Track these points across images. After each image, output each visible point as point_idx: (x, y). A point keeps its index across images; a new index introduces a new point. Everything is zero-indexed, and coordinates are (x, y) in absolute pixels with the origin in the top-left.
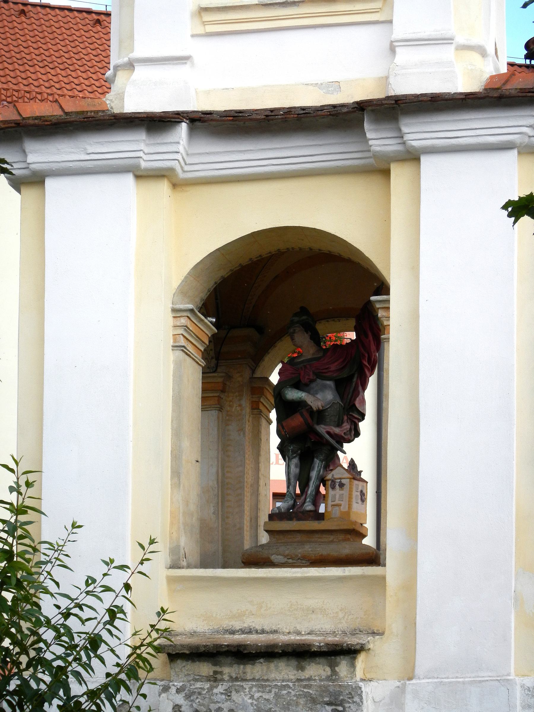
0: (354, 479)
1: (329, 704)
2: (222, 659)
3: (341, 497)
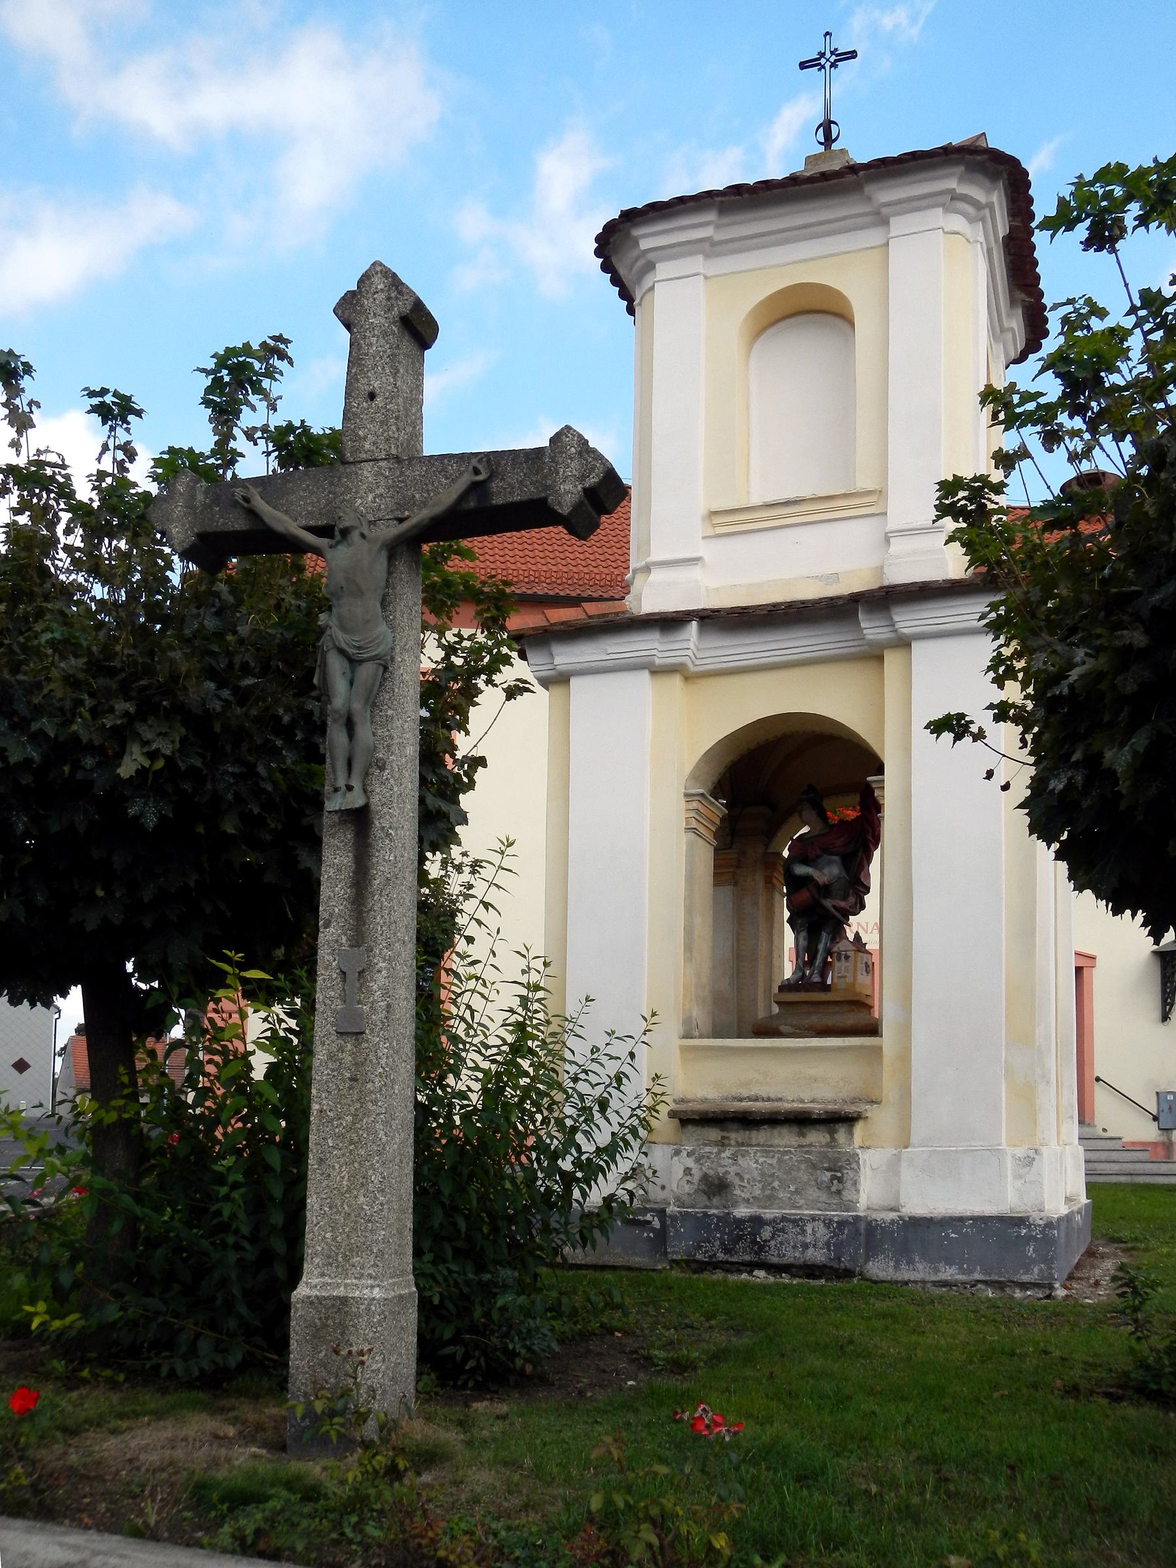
0: (859, 951)
1: (828, 1170)
2: (730, 1125)
3: (847, 969)
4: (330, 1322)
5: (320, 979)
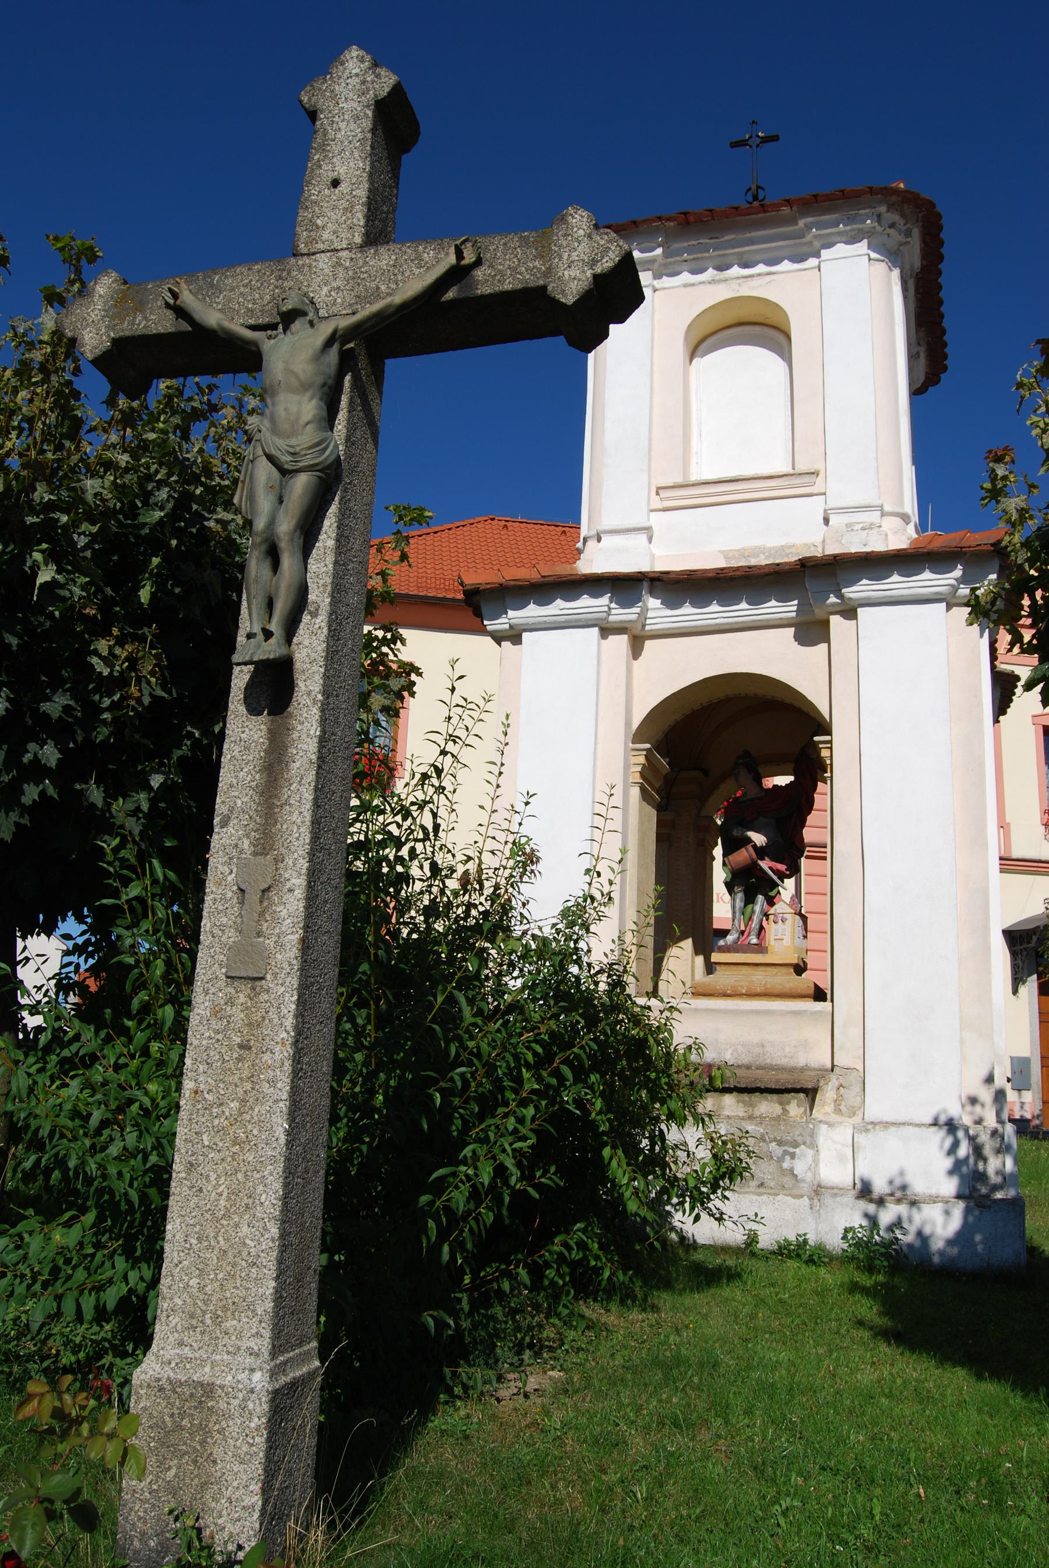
4: (185, 1422)
5: (208, 899)
